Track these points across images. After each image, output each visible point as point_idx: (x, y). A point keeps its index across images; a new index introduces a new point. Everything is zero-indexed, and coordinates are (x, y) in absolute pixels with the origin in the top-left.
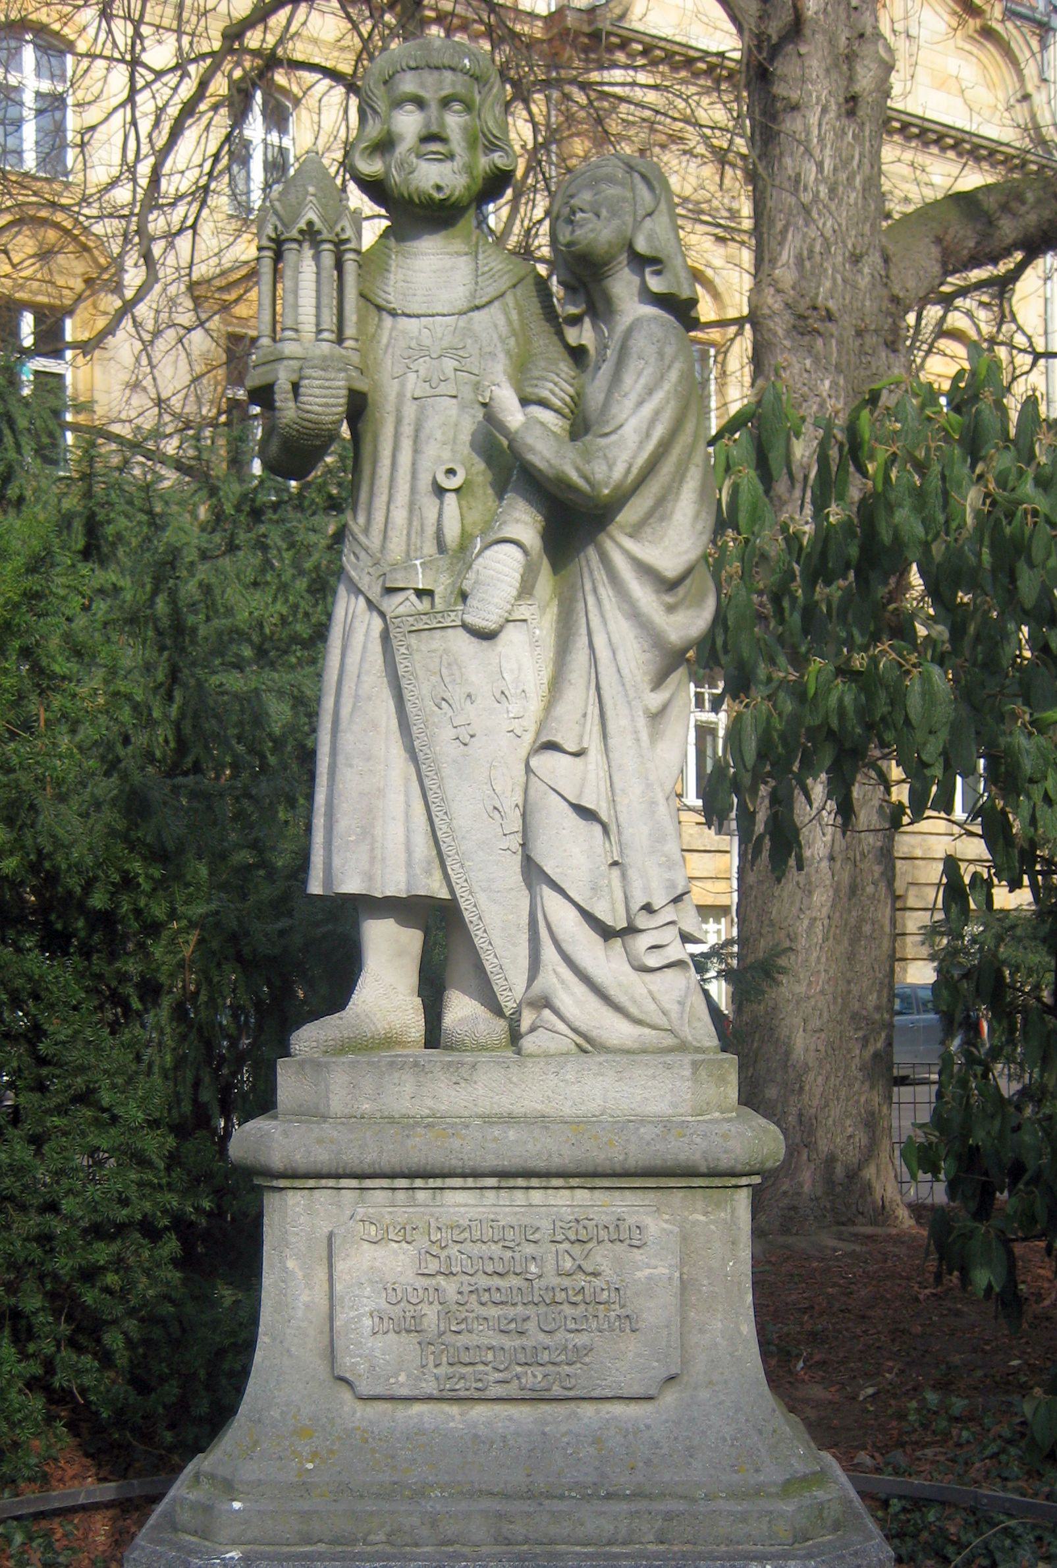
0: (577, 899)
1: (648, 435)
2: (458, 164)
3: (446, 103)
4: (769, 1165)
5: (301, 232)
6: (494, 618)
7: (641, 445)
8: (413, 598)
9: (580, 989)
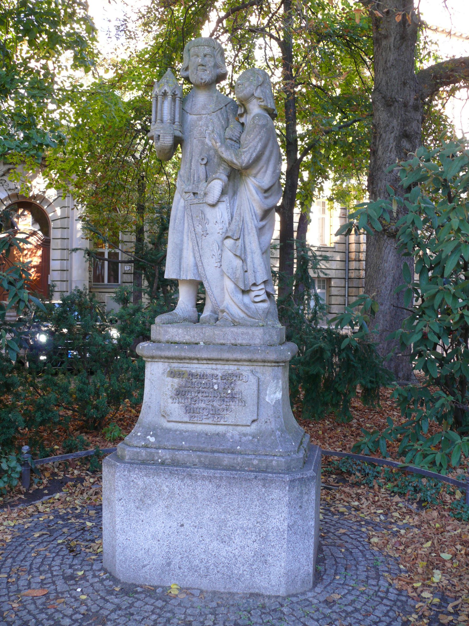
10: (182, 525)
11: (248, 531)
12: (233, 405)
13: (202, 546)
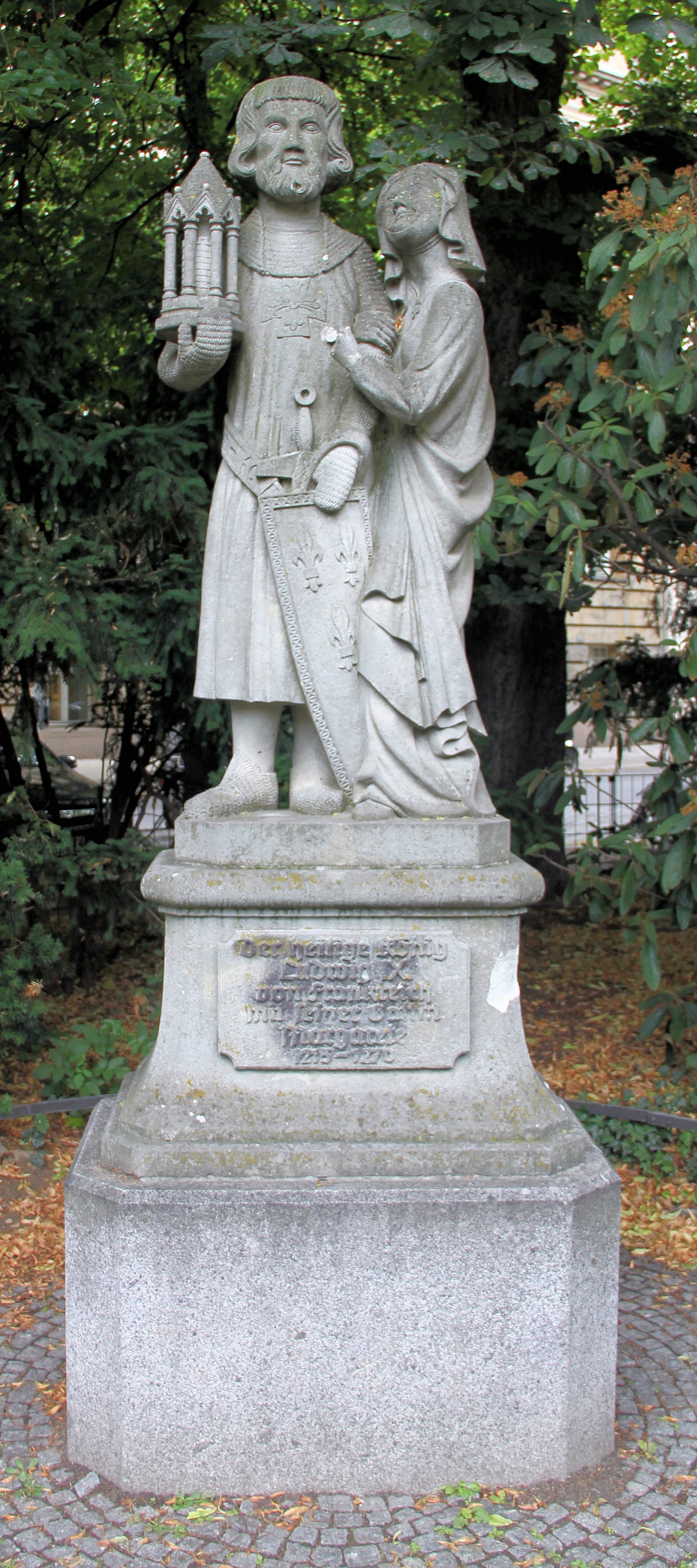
0: (396, 706)
1: (451, 371)
2: (311, 167)
3: (303, 125)
4: (535, 899)
5: (198, 216)
6: (337, 500)
7: (446, 377)
8: (277, 483)
9: (397, 772)
10: (302, 1335)
11: (472, 1334)
12: (410, 1021)
13: (354, 1383)
